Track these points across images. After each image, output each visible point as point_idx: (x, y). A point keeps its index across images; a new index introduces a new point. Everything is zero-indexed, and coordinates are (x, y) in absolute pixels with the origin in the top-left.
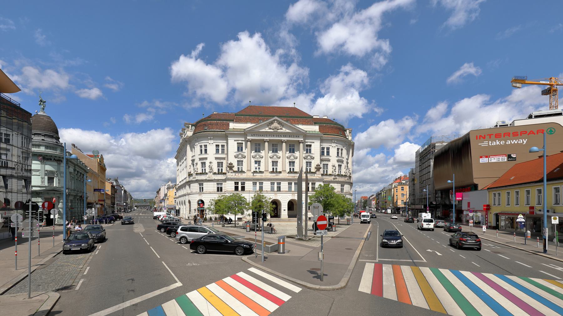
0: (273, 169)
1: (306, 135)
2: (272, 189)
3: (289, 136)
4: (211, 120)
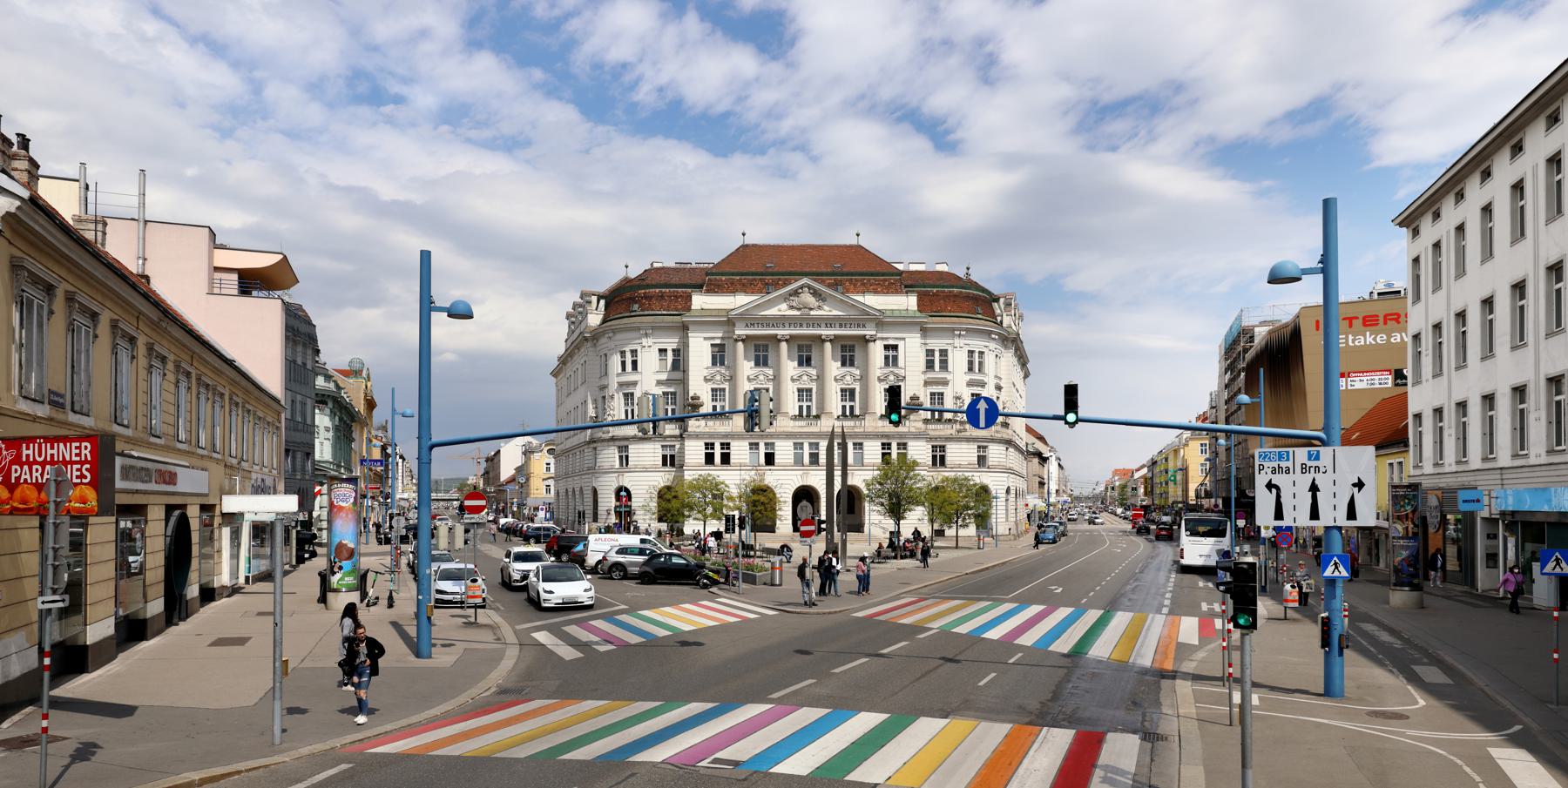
0: (801, 408)
1: (882, 321)
2: (798, 461)
4: (648, 286)
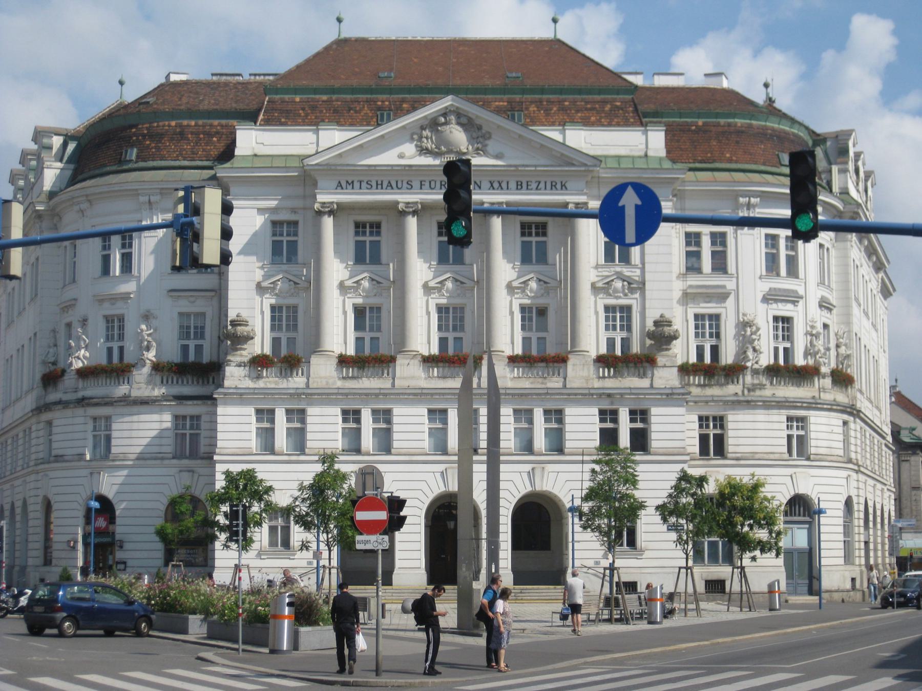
3: (519, 186)
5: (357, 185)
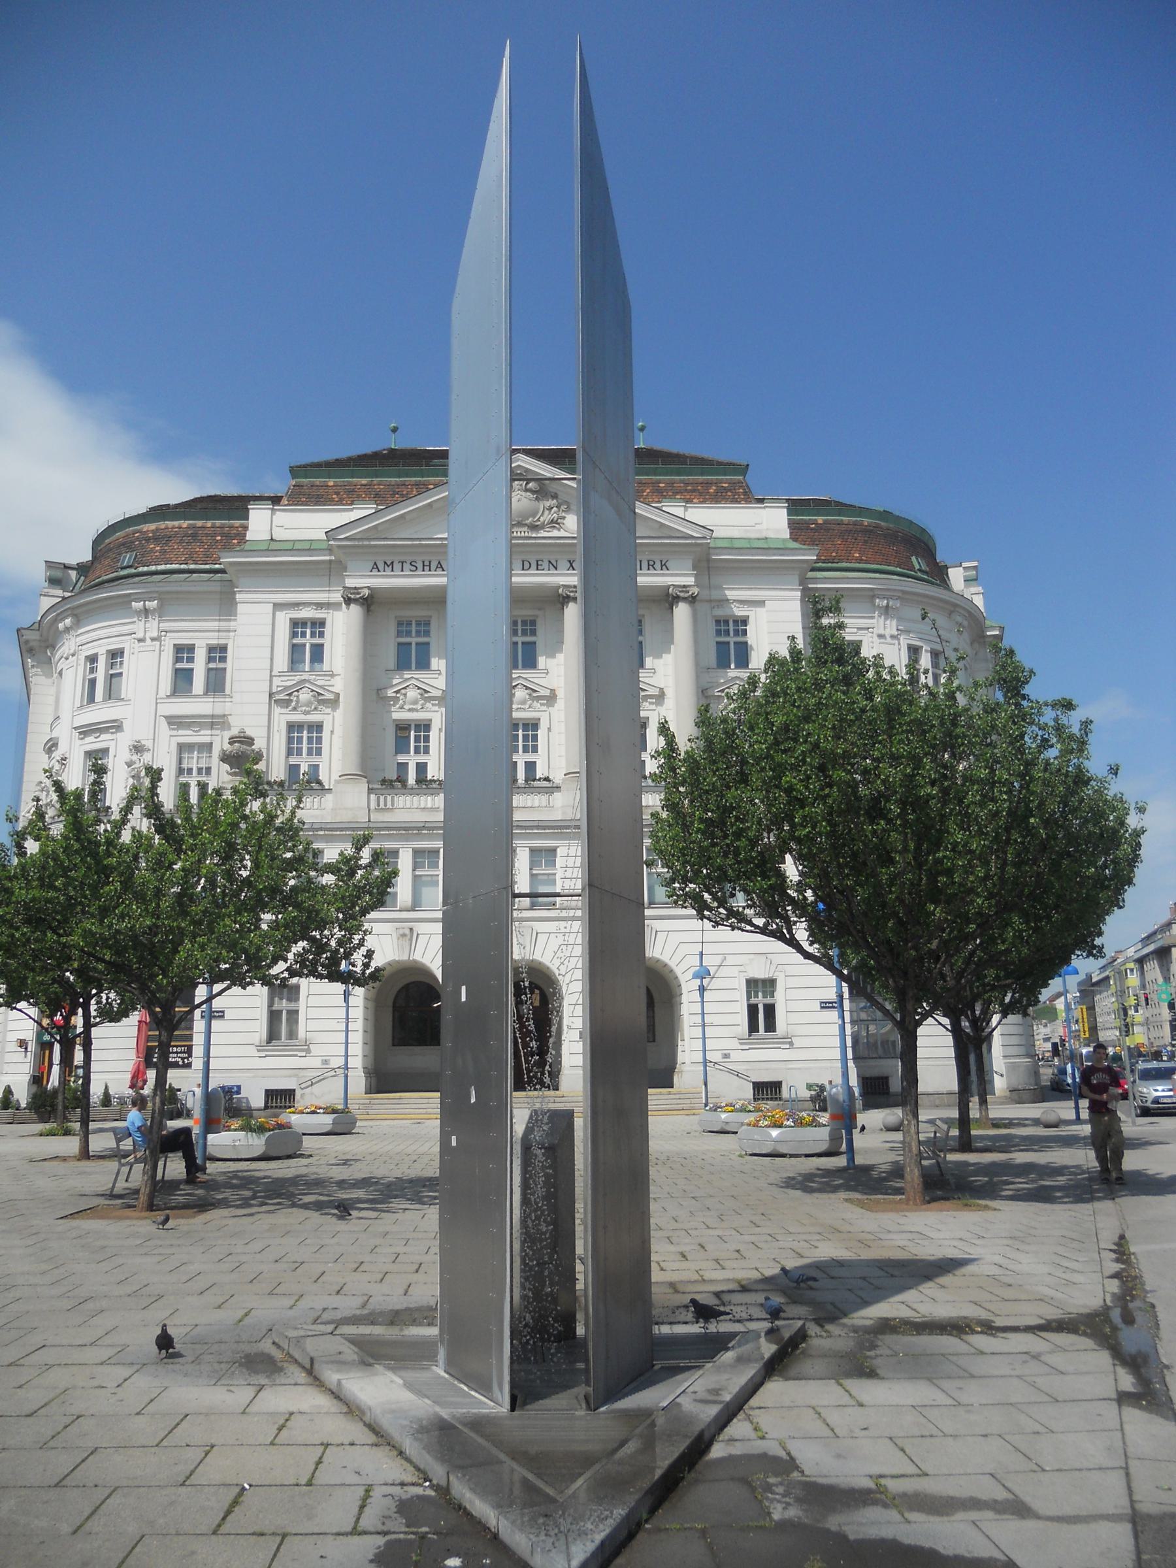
5: (397, 566)
